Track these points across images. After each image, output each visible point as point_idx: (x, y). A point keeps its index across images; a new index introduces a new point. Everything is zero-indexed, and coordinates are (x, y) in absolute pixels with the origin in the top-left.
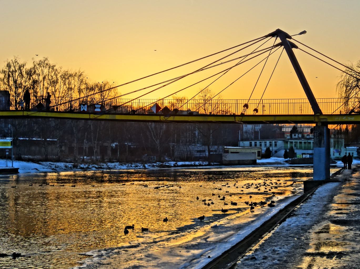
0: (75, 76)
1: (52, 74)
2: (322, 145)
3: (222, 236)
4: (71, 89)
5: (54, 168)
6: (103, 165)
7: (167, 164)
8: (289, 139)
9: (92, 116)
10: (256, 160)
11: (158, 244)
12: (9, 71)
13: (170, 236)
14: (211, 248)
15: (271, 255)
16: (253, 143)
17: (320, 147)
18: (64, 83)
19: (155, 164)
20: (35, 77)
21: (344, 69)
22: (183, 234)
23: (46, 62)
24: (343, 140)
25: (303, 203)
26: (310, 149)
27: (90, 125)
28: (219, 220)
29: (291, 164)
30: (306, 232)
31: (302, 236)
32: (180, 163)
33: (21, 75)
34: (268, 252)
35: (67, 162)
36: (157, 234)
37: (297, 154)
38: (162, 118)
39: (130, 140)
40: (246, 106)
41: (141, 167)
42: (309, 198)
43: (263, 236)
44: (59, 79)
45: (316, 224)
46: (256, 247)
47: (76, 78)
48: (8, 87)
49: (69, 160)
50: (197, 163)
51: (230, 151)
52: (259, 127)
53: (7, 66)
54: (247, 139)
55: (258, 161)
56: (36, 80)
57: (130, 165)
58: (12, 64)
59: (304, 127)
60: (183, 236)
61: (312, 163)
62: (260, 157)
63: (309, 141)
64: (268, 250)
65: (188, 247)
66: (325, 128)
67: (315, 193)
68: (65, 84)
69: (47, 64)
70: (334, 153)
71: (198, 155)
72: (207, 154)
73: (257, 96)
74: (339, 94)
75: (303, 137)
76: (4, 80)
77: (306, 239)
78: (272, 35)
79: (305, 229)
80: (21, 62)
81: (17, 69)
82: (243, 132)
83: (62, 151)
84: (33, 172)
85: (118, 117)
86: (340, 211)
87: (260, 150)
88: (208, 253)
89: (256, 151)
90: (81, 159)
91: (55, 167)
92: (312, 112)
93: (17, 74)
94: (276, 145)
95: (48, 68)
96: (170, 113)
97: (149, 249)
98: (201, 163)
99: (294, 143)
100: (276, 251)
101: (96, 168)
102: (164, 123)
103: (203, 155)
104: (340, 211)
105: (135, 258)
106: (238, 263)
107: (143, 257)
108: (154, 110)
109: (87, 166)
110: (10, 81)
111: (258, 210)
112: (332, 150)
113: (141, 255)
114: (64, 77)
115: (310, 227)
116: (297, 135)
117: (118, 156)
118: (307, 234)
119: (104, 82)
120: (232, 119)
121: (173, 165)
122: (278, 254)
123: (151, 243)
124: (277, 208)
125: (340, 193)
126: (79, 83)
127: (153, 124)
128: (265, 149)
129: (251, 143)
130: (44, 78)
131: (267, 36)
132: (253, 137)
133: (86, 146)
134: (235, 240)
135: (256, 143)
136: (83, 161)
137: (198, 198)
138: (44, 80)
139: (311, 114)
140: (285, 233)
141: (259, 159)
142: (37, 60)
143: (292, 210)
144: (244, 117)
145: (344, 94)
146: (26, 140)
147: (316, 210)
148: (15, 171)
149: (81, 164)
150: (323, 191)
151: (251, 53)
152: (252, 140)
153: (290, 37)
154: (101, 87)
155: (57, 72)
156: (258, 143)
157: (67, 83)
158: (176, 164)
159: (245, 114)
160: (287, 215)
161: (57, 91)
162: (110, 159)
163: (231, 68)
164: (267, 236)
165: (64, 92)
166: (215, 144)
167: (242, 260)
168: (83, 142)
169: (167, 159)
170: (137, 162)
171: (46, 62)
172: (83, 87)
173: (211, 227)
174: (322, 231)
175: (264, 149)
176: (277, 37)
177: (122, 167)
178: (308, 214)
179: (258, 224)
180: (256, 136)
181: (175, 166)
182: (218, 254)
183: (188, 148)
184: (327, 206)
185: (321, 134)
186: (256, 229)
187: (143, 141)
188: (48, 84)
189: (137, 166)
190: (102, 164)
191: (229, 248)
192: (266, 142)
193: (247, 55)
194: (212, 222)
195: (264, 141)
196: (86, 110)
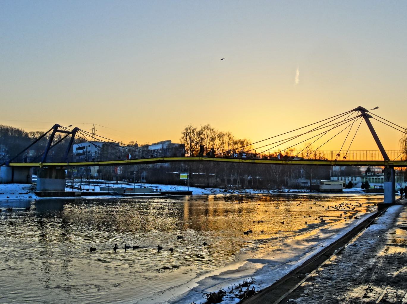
0: (226, 135)
1: (212, 134)
2: (390, 180)
3: (328, 235)
4: (224, 143)
5: (213, 192)
6: (243, 191)
7: (283, 191)
8: (364, 176)
9: (241, 161)
10: (342, 190)
11: (289, 238)
12: (187, 133)
13: (295, 234)
14: (322, 241)
15: (365, 244)
16: (340, 178)
17: (389, 182)
18: (219, 140)
19: (275, 191)
20: (202, 136)
21: (404, 130)
22: (303, 233)
23: (209, 127)
24: (404, 177)
25: (379, 216)
26: (380, 183)
27: (235, 166)
28: (323, 226)
29: (366, 192)
30: (384, 233)
31: (382, 235)
32: (291, 190)
33: (194, 135)
34: (362, 242)
35: (221, 188)
36: (287, 232)
37: (371, 186)
38: (284, 162)
39: (259, 175)
40: (338, 155)
41: (267, 192)
42: (382, 214)
43: (357, 234)
44: (217, 137)
45: (390, 229)
46: (355, 239)
47: (227, 136)
48: (186, 142)
49: (222, 187)
50: (303, 190)
51: (325, 183)
52: (343, 168)
53: (186, 129)
54: (335, 176)
55: (343, 190)
56: (202, 137)
57: (260, 191)
58: (188, 128)
59: (375, 168)
60: (303, 234)
61: (383, 192)
62: (345, 188)
63: (379, 177)
64: (363, 241)
65: (308, 240)
66: (392, 169)
67: (386, 211)
68: (220, 140)
69: (209, 128)
70: (398, 187)
71: (303, 185)
72: (309, 184)
73: (345, 148)
74: (400, 146)
75: (374, 175)
76: (183, 138)
77: (385, 237)
78: (356, 110)
79: (383, 232)
80: (194, 127)
81: (191, 131)
82: (333, 171)
83: (217, 181)
84: (201, 194)
85: (256, 161)
86: (405, 222)
87: (345, 183)
88: (321, 244)
89: (342, 183)
90: (229, 186)
91: (214, 191)
92: (383, 160)
93: (191, 134)
94: (355, 180)
95: (209, 130)
96: (289, 159)
97: (284, 240)
98: (305, 190)
99: (368, 179)
100: (368, 242)
101: (238, 192)
102: (182, 162)
103: (306, 185)
104: (405, 222)
105: (277, 245)
106: (345, 247)
107: (281, 245)
108: (279, 157)
109: (233, 191)
110: (187, 138)
111: (349, 221)
112: (396, 184)
113: (280, 243)
114: (219, 136)
115: (387, 230)
116: (370, 173)
117: (252, 185)
118: (385, 234)
119: (244, 139)
120: (329, 163)
121: (287, 192)
122: (369, 244)
123: (284, 237)
124: (361, 220)
125: (404, 212)
126: (229, 139)
127: (274, 166)
128: (348, 182)
129: (338, 178)
130: (207, 136)
131: (352, 111)
132: (340, 174)
133: (232, 179)
134: (336, 237)
135: (342, 178)
136: (230, 188)
137: (160, 248)
138: (207, 138)
139: (382, 160)
140: (371, 233)
141: (344, 189)
142: (203, 126)
143: (373, 220)
144: (337, 162)
145: (404, 146)
146: (196, 174)
147: (389, 221)
148: (190, 193)
149: (229, 190)
150: (392, 210)
151: (342, 121)
152: (339, 176)
153: (368, 112)
154: (242, 142)
155: (215, 133)
156: (343, 178)
157: (221, 139)
158: (289, 191)
159: (338, 160)
160: (370, 223)
161: (215, 144)
162: (247, 187)
163: (329, 130)
164: (360, 234)
165: (219, 145)
166: (314, 178)
167: (347, 246)
168: (230, 176)
169: (283, 187)
170: (264, 189)
171: (209, 127)
172: (231, 142)
173: (320, 230)
174: (327, 279)
175: (347, 182)
176: (359, 111)
177: (255, 192)
178: (384, 223)
179: (350, 229)
180: (341, 174)
181: (288, 192)
182: (327, 245)
183: (297, 181)
184: (396, 219)
185: (389, 173)
186: (354, 228)
187: (268, 176)
188: (210, 140)
189: (264, 192)
190: (242, 190)
191: (334, 242)
192: (348, 178)
193: (340, 123)
194: (320, 227)
195: (347, 177)
196: (237, 157)
